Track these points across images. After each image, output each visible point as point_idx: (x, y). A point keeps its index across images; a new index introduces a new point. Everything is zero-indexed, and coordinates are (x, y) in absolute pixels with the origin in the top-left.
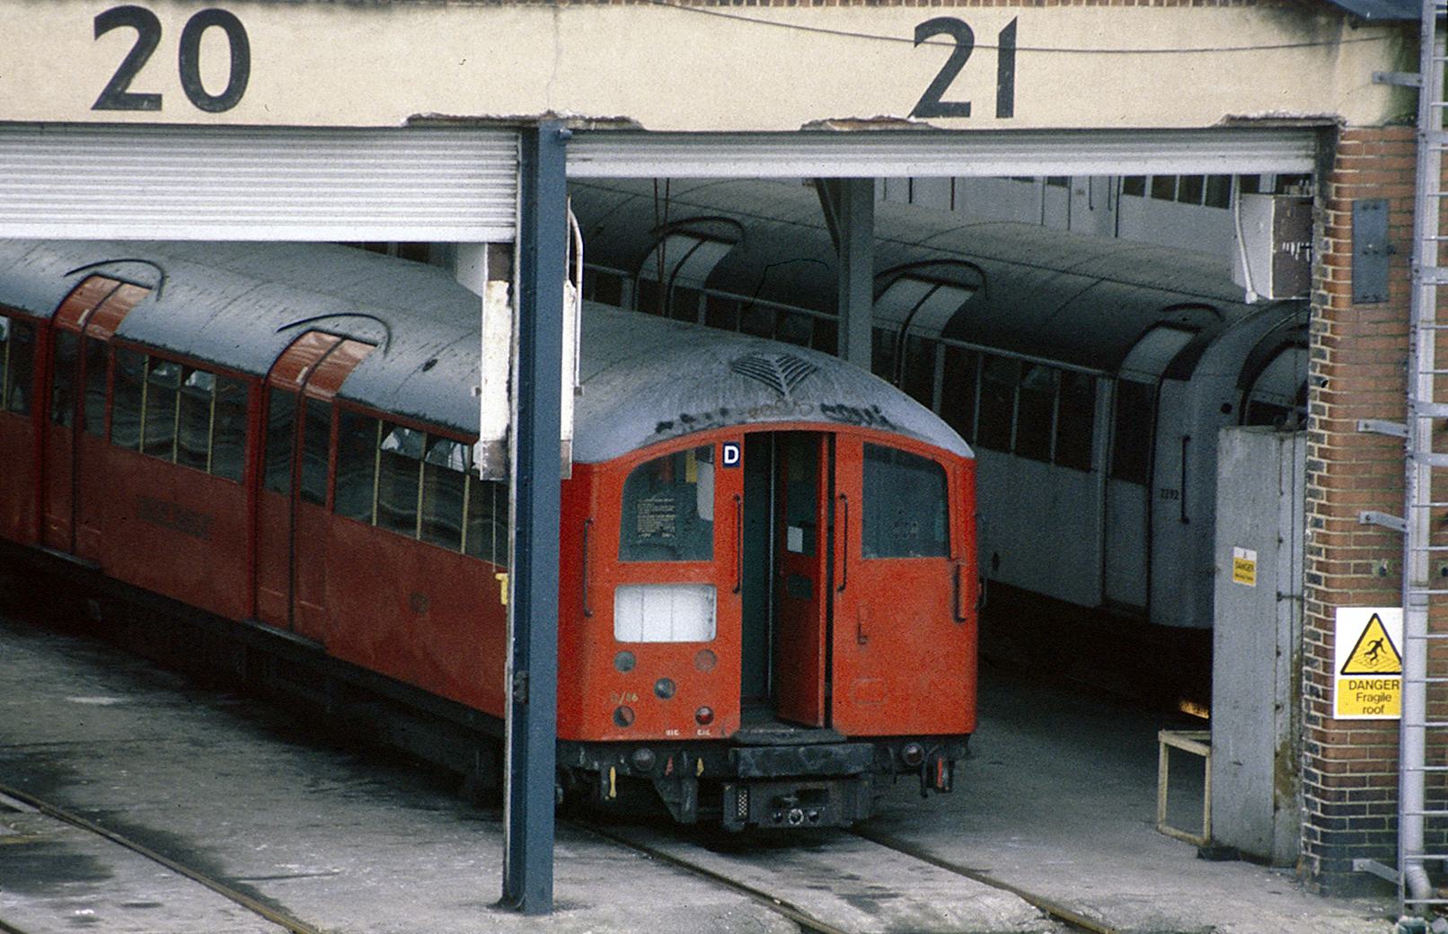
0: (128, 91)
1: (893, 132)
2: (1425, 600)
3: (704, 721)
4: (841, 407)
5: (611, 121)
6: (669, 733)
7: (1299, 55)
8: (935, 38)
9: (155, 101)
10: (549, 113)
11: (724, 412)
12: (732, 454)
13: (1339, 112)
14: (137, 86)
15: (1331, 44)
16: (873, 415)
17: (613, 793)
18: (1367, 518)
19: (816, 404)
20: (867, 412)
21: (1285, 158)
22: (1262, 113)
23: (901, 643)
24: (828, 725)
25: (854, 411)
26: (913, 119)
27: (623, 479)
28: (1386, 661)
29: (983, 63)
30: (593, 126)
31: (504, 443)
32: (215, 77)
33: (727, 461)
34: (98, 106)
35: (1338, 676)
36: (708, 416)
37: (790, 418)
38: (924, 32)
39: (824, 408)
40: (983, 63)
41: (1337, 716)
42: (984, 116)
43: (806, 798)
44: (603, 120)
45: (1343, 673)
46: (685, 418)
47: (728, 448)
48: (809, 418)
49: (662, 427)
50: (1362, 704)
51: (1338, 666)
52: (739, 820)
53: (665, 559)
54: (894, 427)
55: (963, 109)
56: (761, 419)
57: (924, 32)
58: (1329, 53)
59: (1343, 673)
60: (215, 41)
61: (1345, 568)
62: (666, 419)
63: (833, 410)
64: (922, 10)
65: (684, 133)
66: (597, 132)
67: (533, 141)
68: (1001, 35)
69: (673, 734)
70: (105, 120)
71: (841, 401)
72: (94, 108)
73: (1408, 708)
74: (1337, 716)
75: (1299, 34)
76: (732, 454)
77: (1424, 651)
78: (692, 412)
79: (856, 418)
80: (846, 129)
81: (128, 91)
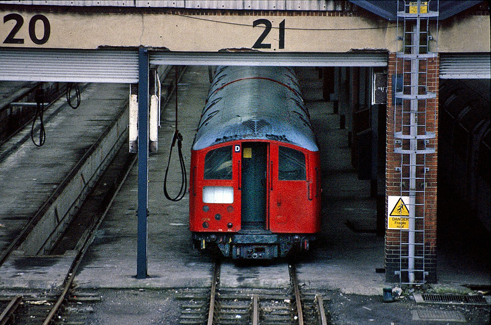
0: (14, 38)
1: (248, 53)
2: (414, 194)
3: (230, 227)
4: (272, 135)
5: (160, 48)
6: (219, 230)
7: (374, 31)
8: (260, 25)
9: (22, 41)
10: (141, 46)
11: (236, 136)
12: (237, 149)
13: (387, 48)
14: (16, 37)
15: (384, 28)
16: (283, 138)
17: (204, 247)
18: (398, 169)
19: (265, 134)
20: (281, 137)
21: (378, 62)
22: (363, 48)
23: (297, 207)
24: (269, 229)
25: (277, 136)
26: (253, 49)
27: (205, 155)
28: (404, 212)
29: (274, 33)
30: (156, 50)
31: (136, 142)
32: (40, 33)
33: (236, 150)
34: (5, 42)
35: (389, 216)
36: (231, 137)
37: (256, 138)
38: (256, 23)
39: (267, 135)
40: (274, 33)
41: (389, 228)
42: (275, 47)
43: (258, 250)
44: (158, 48)
45: (390, 215)
46: (225, 138)
47: (236, 147)
48: (262, 138)
49: (218, 140)
50: (397, 225)
51: (389, 214)
52: (237, 256)
53: (219, 179)
54: (289, 141)
55: (269, 46)
56: (246, 138)
57: (256, 23)
58: (384, 31)
59: (390, 215)
60: (40, 24)
61: (391, 184)
62: (219, 138)
63: (269, 136)
64: (255, 17)
65: (183, 52)
66: (157, 51)
67: (144, 55)
68: (280, 24)
69: (221, 230)
70: (12, 46)
71: (273, 133)
72: (4, 43)
73: (409, 226)
74: (389, 228)
75: (374, 25)
76: (237, 149)
77: (414, 209)
78: (227, 136)
79: (276, 138)
80: (233, 51)
81: (14, 38)
